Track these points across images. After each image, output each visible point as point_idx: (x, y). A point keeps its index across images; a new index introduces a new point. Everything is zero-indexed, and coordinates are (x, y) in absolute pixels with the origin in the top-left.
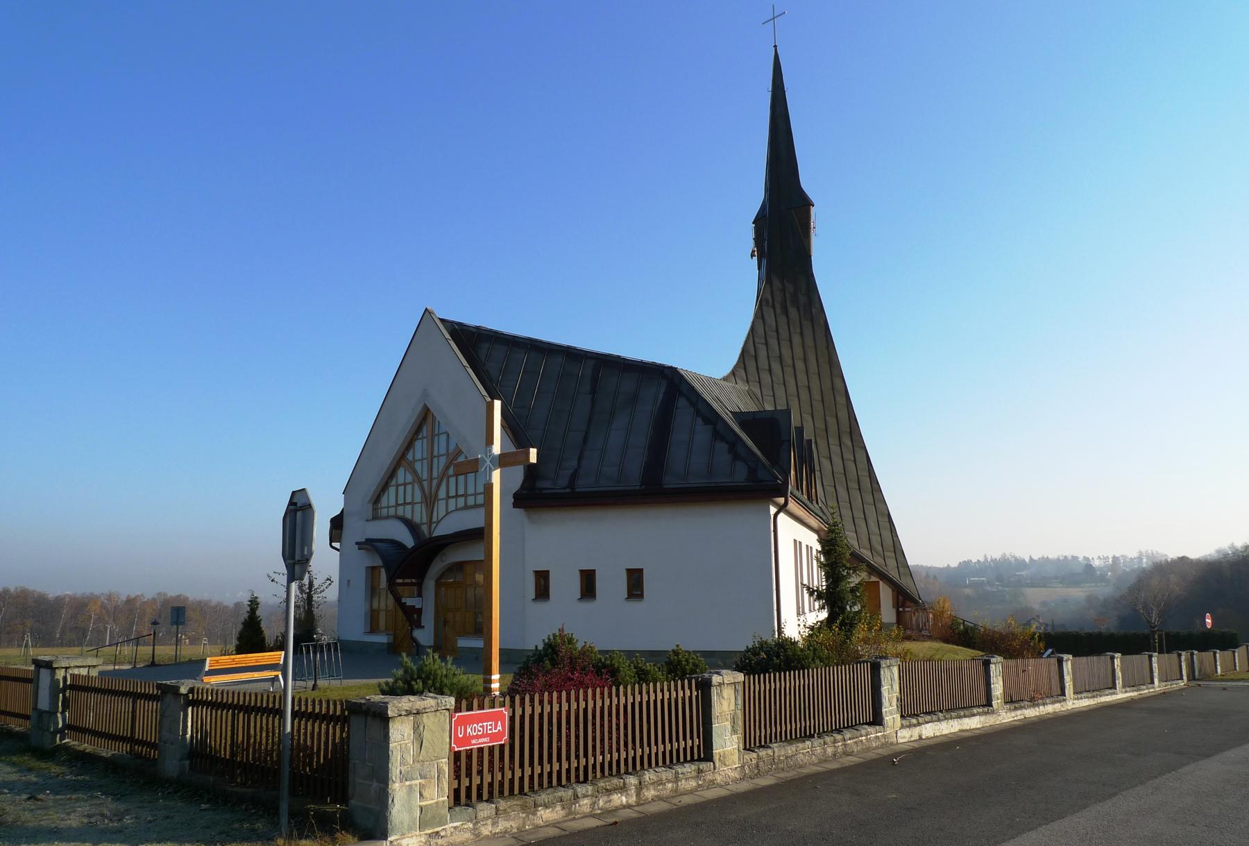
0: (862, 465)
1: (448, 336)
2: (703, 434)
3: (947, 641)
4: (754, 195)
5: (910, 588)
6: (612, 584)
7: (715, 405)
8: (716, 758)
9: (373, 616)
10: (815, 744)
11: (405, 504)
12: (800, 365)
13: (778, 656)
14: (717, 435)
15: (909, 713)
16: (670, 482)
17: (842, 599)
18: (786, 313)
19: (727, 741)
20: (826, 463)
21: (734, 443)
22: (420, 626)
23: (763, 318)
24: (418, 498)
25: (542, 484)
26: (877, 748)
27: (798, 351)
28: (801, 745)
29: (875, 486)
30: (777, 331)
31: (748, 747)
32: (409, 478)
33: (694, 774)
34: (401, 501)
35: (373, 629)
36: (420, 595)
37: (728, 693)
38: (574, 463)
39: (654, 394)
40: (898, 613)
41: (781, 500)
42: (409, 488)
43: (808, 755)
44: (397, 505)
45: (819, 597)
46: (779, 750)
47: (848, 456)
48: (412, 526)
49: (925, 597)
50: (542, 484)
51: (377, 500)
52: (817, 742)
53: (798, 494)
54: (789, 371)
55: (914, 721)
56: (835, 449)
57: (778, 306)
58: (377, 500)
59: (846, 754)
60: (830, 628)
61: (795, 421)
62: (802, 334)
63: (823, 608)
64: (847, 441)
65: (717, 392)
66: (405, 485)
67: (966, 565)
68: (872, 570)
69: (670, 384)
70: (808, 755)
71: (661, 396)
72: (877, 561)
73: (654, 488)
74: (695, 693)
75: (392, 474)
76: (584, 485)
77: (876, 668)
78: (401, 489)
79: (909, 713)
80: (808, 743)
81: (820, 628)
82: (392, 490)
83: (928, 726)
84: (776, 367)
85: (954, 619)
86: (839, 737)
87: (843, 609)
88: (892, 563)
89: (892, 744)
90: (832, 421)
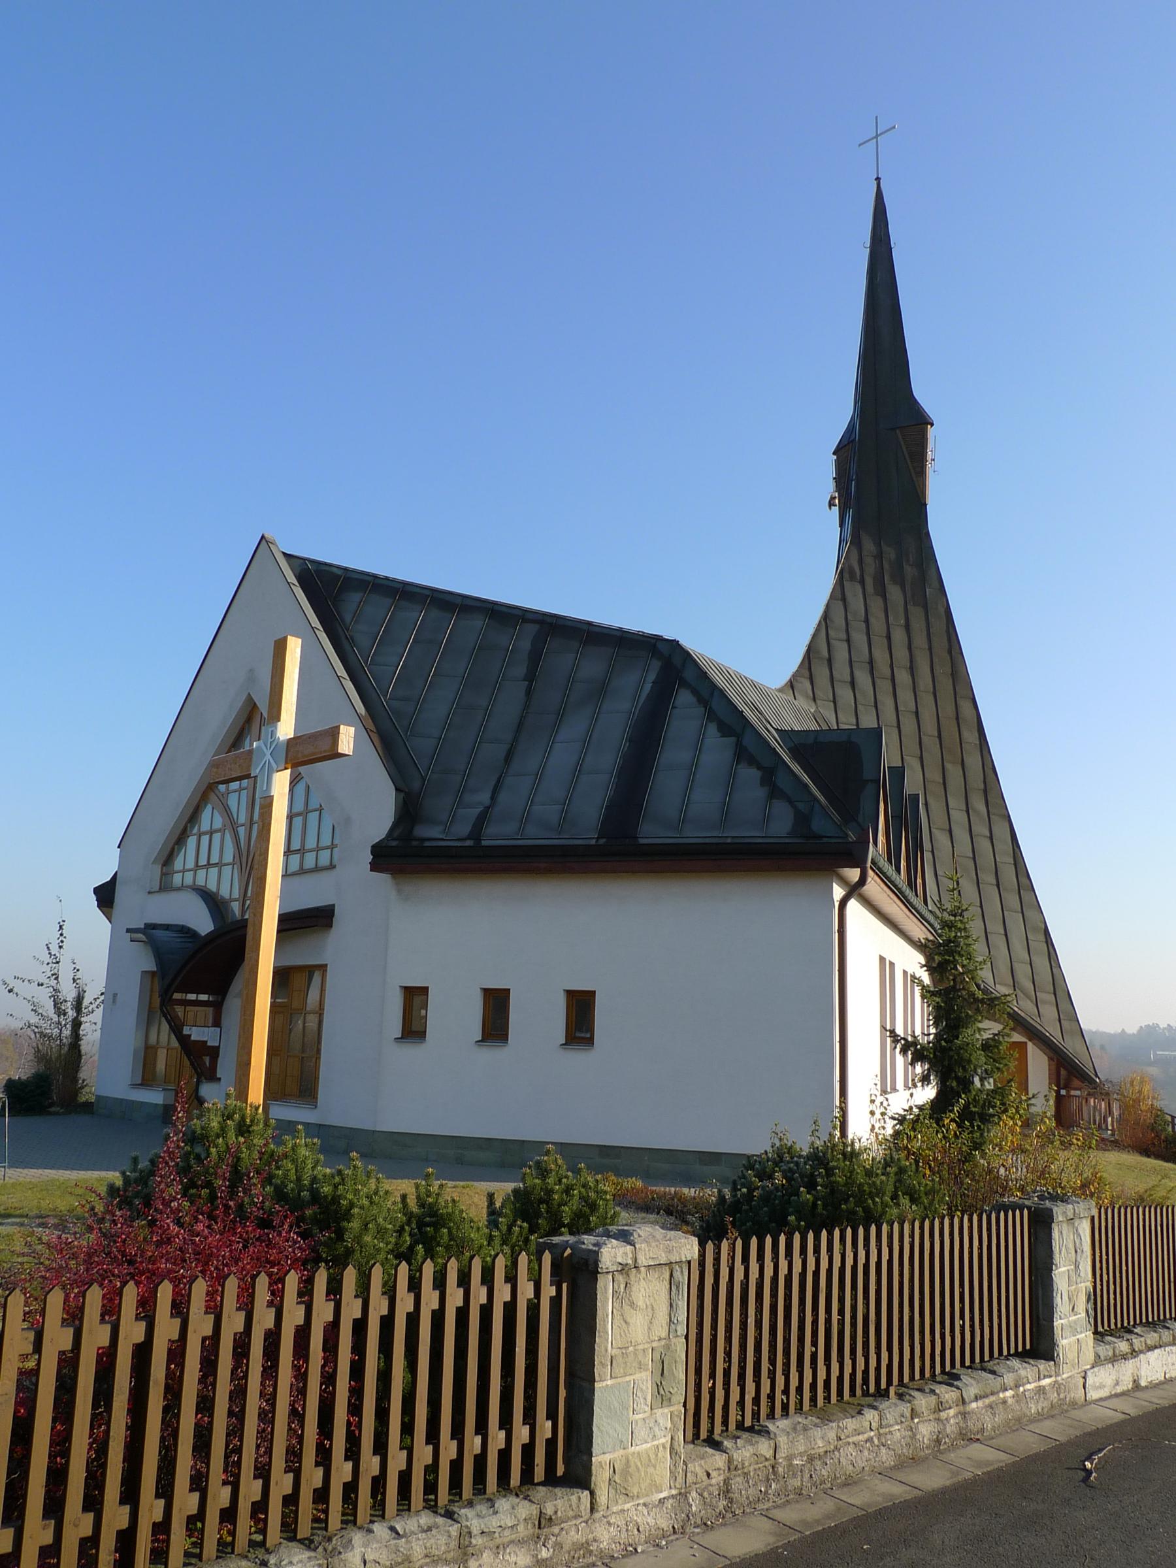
0: (1004, 846)
1: (292, 579)
2: (717, 750)
3: (1146, 1152)
4: (836, 410)
5: (1081, 1058)
6: (538, 1017)
7: (748, 713)
8: (600, 1477)
9: (148, 1054)
10: (890, 1417)
11: (209, 865)
12: (903, 677)
13: (811, 1186)
14: (742, 755)
15: (1113, 1322)
16: (651, 833)
17: (964, 1063)
18: (882, 592)
19: (637, 1422)
20: (942, 839)
21: (771, 771)
22: (212, 1077)
23: (844, 599)
24: (229, 857)
25: (421, 831)
26: (1040, 1417)
27: (901, 654)
28: (850, 1424)
29: (1023, 880)
30: (867, 621)
31: (704, 1428)
32: (218, 822)
33: (523, 1531)
34: (203, 861)
35: (147, 1080)
36: (217, 1023)
37: (650, 1292)
38: (485, 797)
39: (635, 684)
40: (1059, 1099)
41: (854, 874)
42: (217, 837)
43: (868, 1450)
44: (197, 866)
45: (919, 1056)
46: (794, 1440)
47: (981, 829)
48: (213, 901)
49: (1105, 1068)
50: (421, 831)
51: (168, 860)
52: (893, 1409)
53: (890, 870)
54: (884, 686)
55: (1123, 1346)
56: (958, 816)
57: (869, 581)
58: (168, 860)
59: (968, 1437)
60: (938, 1121)
61: (890, 755)
62: (907, 627)
63: (925, 1079)
64: (979, 805)
65: (753, 696)
66: (211, 833)
67: (1149, 1031)
68: (1019, 1022)
69: (669, 668)
70: (868, 1450)
71: (648, 687)
72: (1024, 1007)
73: (623, 845)
74: (549, 1291)
75: (193, 816)
76: (498, 834)
77: (1041, 1223)
78: (205, 839)
79: (1113, 1322)
80: (870, 1415)
81: (916, 1120)
82: (191, 842)
83: (1153, 1355)
84: (863, 678)
85: (1158, 1114)
86: (947, 1394)
87: (966, 1084)
88: (1049, 1012)
89: (1074, 1404)
90: (954, 771)
